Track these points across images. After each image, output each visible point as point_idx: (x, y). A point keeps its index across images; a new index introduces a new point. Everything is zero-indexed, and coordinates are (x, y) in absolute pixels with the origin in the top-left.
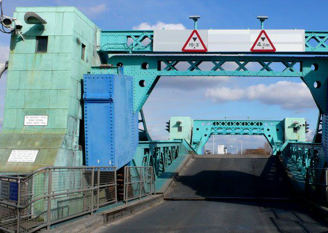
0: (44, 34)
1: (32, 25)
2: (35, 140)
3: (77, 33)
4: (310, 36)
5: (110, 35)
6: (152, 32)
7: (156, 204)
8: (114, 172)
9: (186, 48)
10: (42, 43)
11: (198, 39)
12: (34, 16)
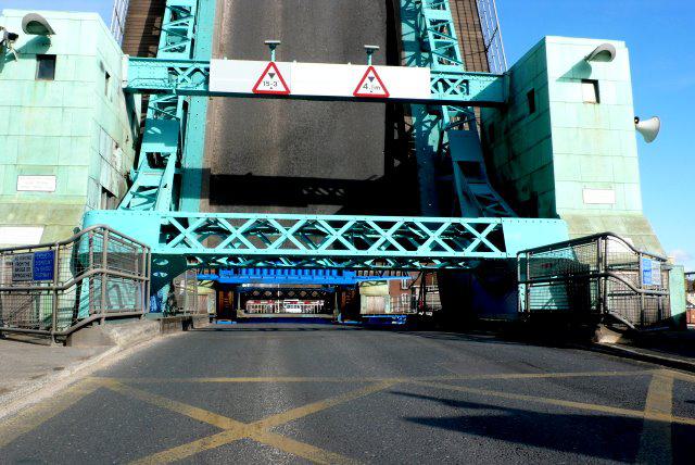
0: (50, 52)
1: (34, 36)
2: (37, 213)
3: (78, 293)
4: (437, 77)
6: (208, 63)
7: (523, 304)
10: (47, 65)
11: (276, 77)
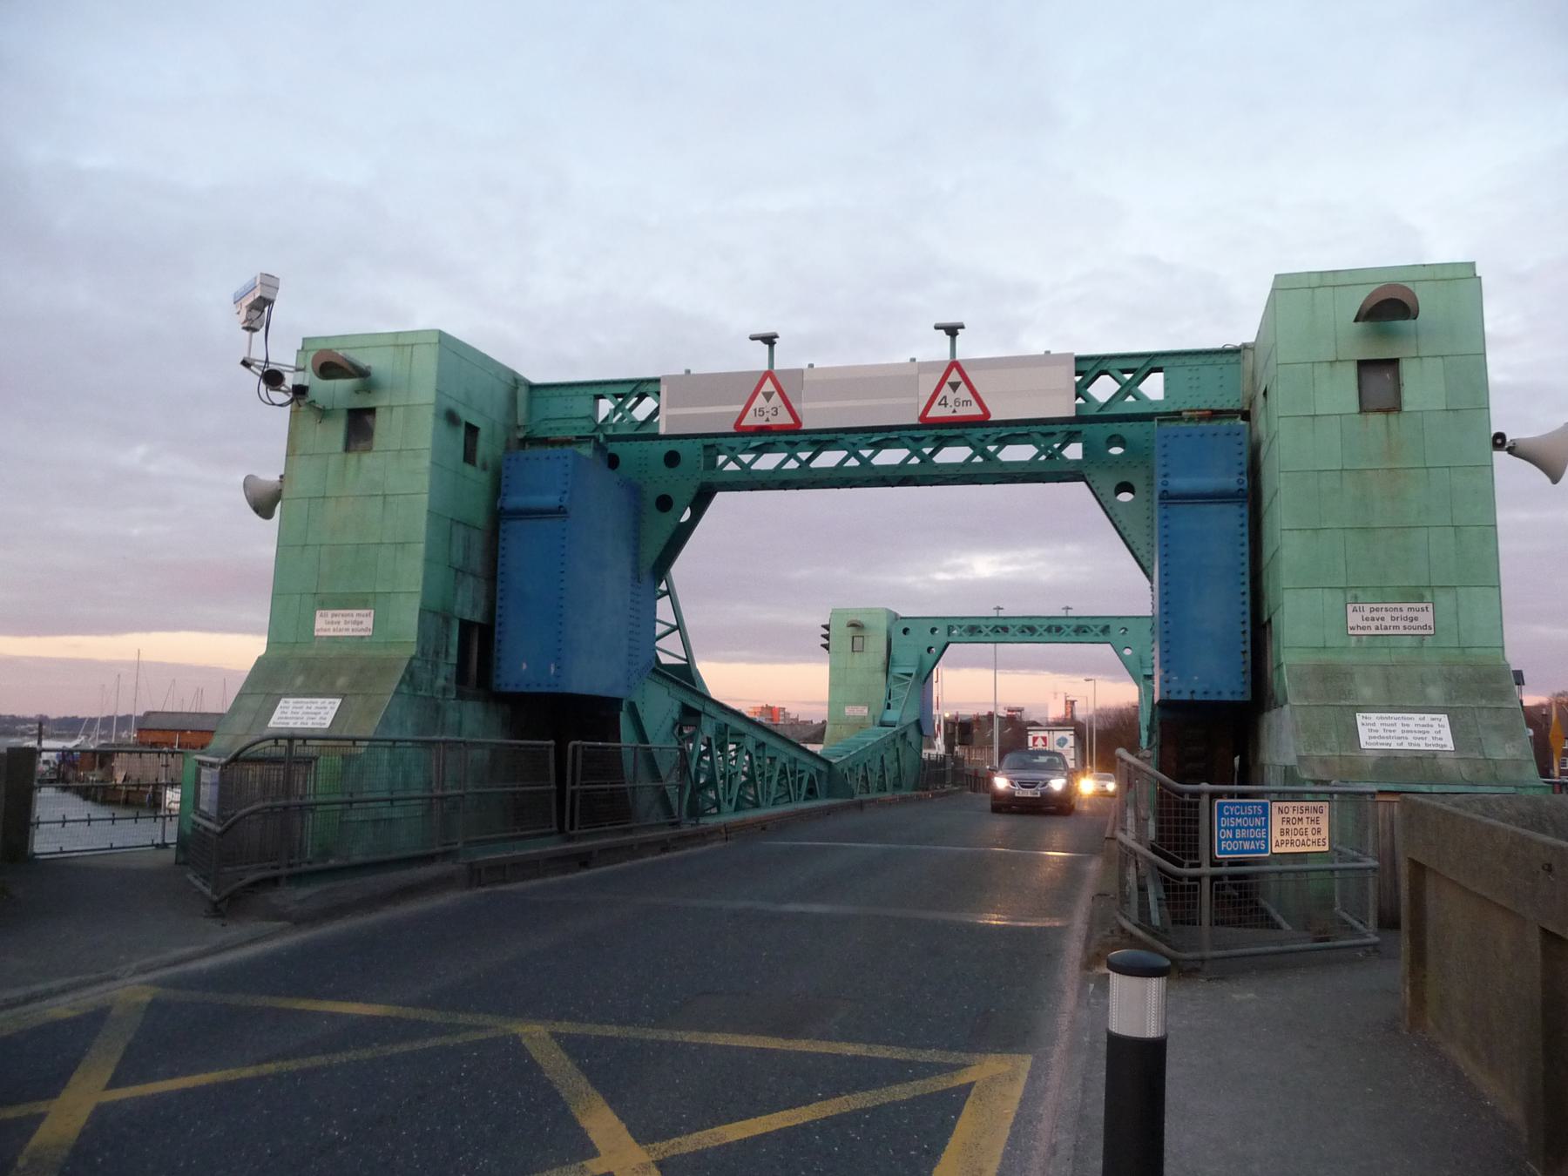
8: (620, 742)
9: (931, 414)
12: (334, 360)
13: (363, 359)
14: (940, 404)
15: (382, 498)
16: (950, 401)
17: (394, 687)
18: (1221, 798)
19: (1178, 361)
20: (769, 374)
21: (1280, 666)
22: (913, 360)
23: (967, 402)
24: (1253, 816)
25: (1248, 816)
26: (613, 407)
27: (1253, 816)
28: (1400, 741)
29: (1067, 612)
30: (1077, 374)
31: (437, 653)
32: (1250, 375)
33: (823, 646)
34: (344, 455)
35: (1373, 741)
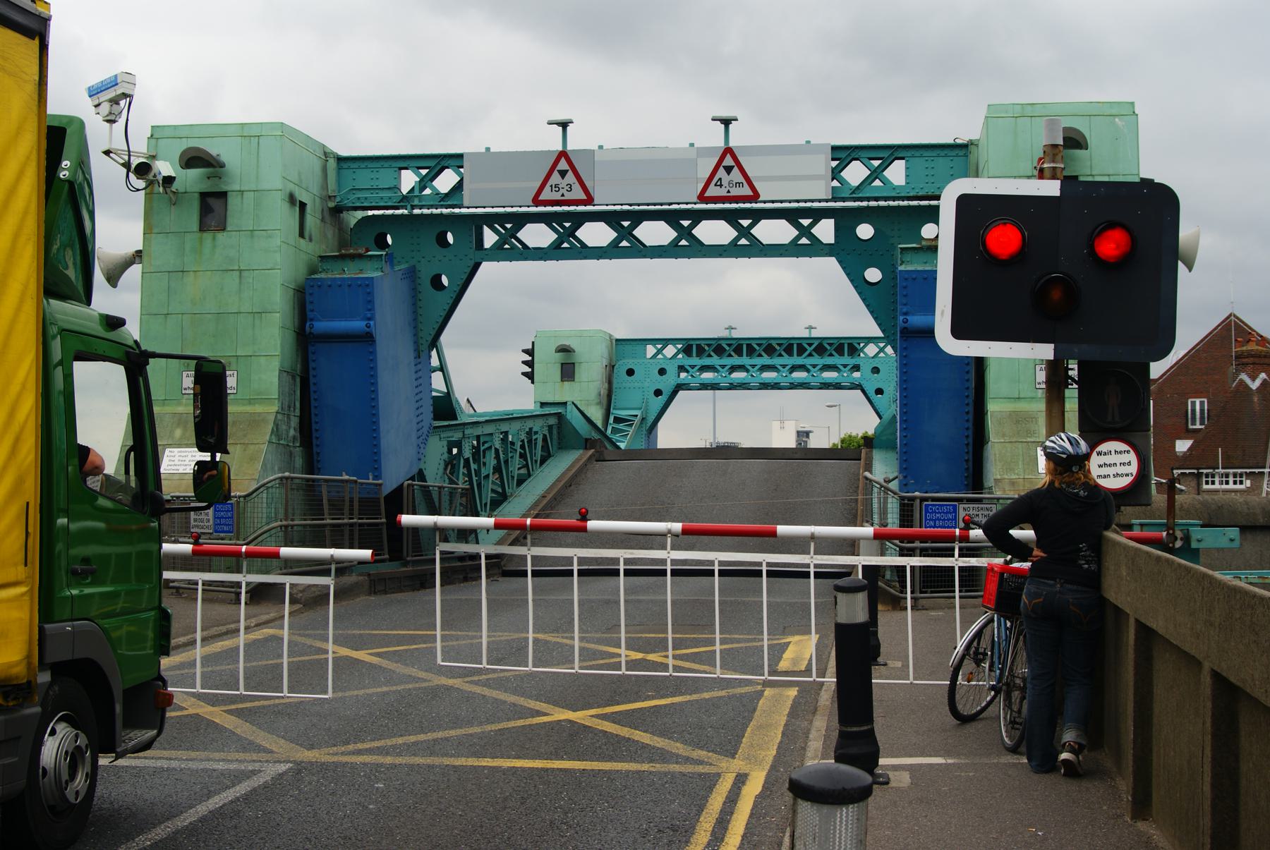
5: (359, 168)
13: (213, 148)
14: (716, 185)
15: (238, 273)
16: (725, 183)
17: (268, 438)
18: (928, 501)
19: (912, 152)
20: (563, 154)
21: (987, 411)
22: (692, 145)
23: (739, 184)
24: (947, 513)
25: (944, 513)
26: (418, 180)
27: (947, 513)
28: (185, 468)
29: (810, 333)
30: (833, 159)
31: (289, 407)
32: (975, 168)
33: (524, 374)
34: (199, 235)
35: (170, 467)
